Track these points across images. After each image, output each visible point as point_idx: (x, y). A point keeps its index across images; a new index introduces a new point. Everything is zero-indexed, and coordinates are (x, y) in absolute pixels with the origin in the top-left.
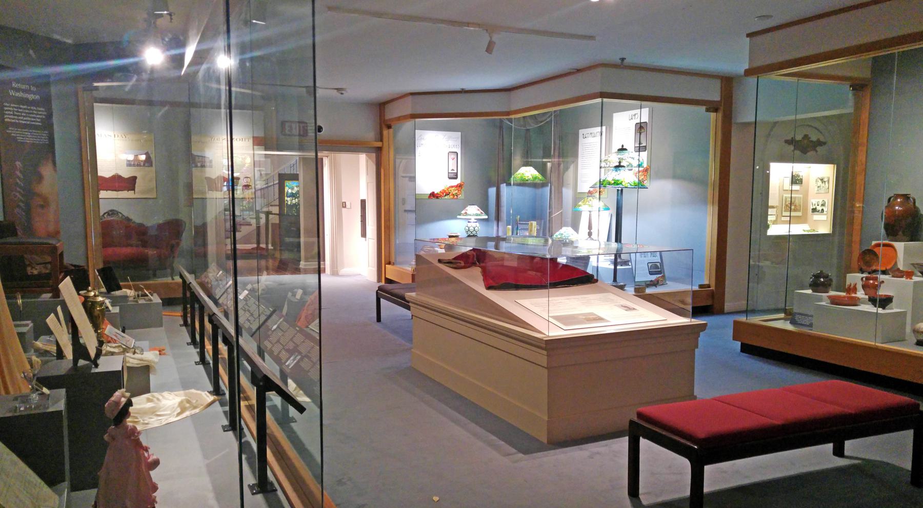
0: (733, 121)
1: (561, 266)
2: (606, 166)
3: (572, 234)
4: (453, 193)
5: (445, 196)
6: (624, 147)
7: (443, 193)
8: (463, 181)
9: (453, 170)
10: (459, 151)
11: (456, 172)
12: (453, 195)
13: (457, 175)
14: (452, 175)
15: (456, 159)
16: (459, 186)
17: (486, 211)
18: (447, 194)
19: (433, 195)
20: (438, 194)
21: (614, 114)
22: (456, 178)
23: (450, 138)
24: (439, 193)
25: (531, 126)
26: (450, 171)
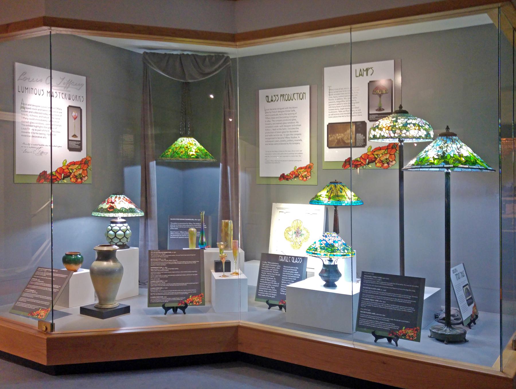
0: (399, 114)
1: (6, 116)
2: (392, 135)
3: (27, 147)
4: (196, 301)
5: (368, 164)
6: (403, 109)
7: (365, 160)
8: (90, 155)
9: (75, 136)
10: (83, 106)
11: (79, 139)
12: (196, 302)
13: (81, 145)
14: (74, 145)
15: (79, 118)
16: (84, 163)
17: (146, 206)
18: (371, 161)
19: (283, 177)
20: (287, 176)
21: (327, 70)
22: (80, 150)
23: (70, 83)
24: (359, 159)
25: (193, 78)
26: (71, 138)
